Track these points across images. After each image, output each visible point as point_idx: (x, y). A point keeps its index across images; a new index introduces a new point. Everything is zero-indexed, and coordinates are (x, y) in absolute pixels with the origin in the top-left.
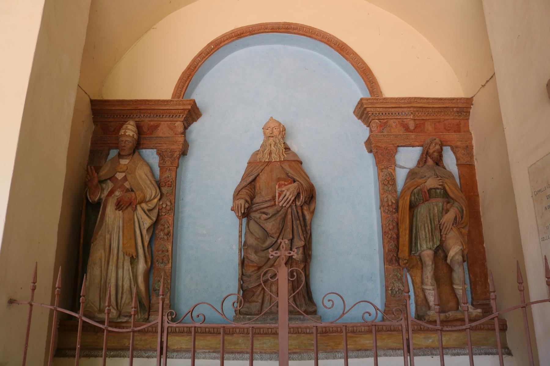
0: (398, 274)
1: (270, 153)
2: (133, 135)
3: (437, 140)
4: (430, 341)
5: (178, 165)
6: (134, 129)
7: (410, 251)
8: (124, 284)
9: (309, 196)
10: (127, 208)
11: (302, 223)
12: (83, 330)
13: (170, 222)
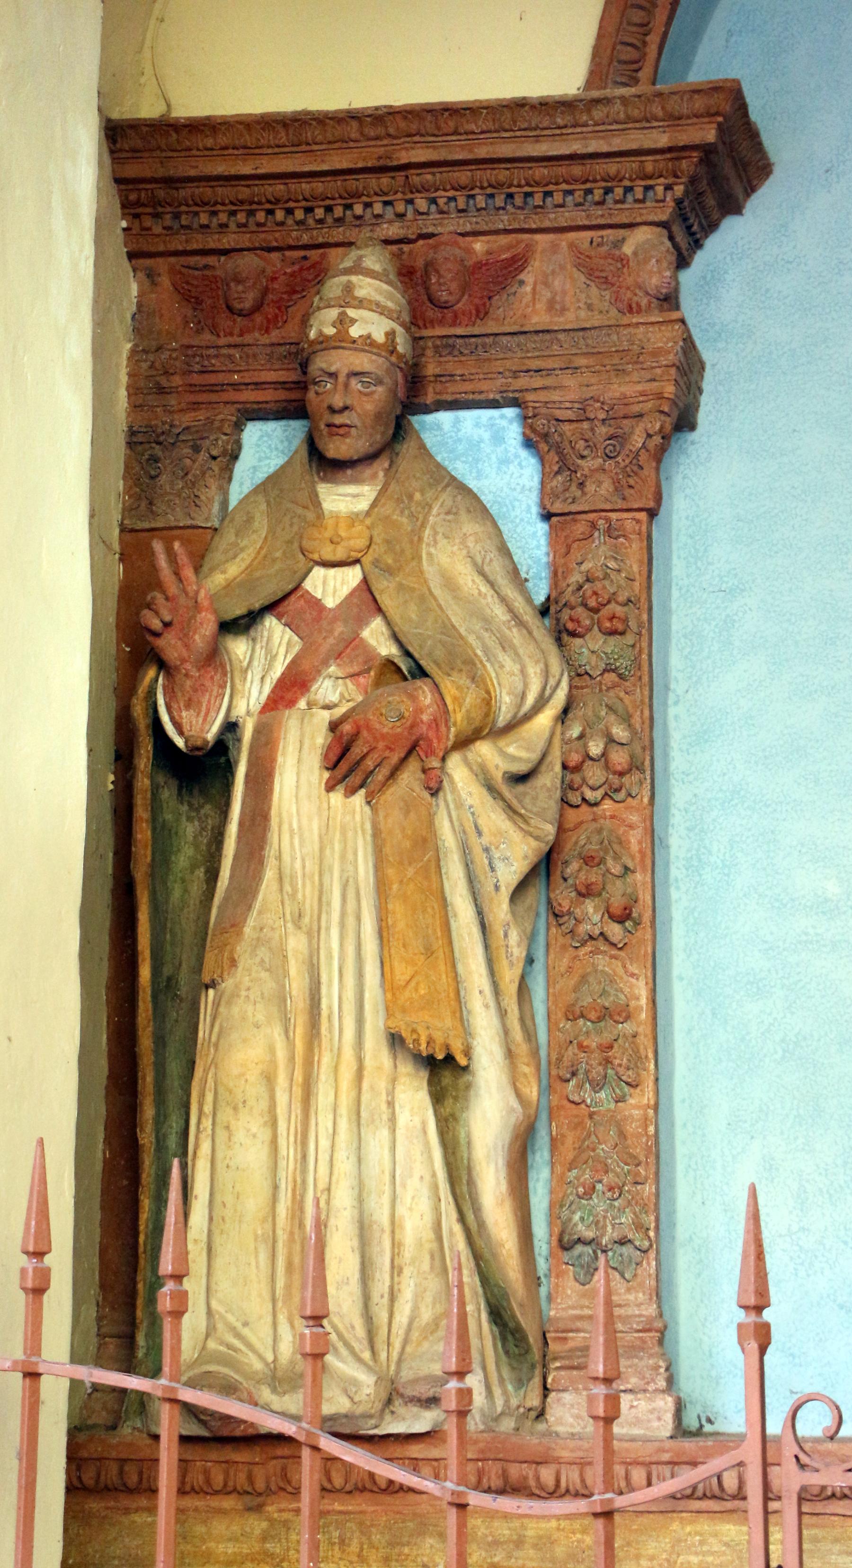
2: (391, 335)
5: (658, 498)
8: (401, 1210)
13: (634, 839)
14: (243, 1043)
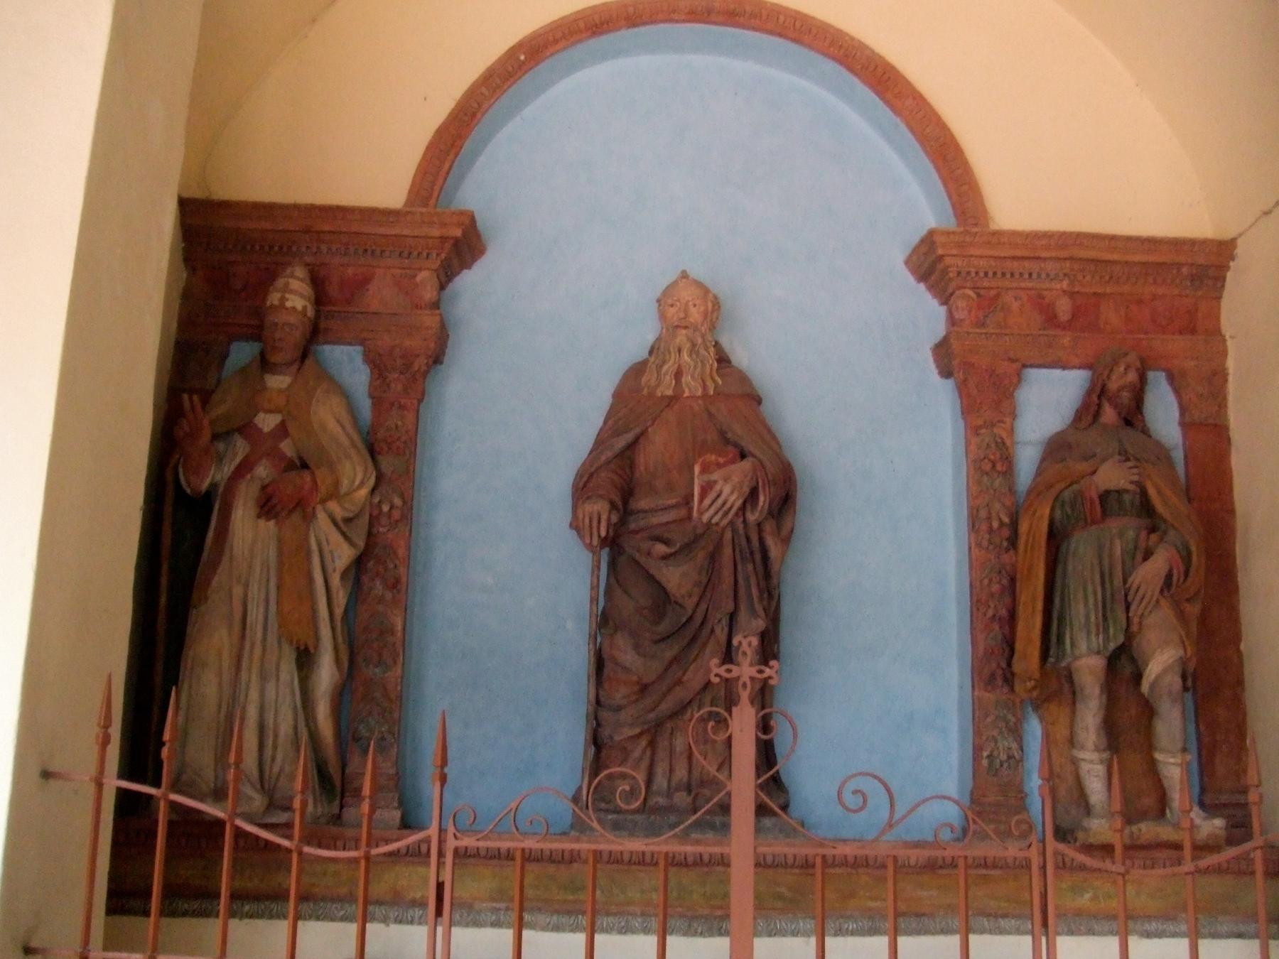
0: (1010, 717)
1: (678, 375)
2: (305, 308)
3: (1132, 358)
4: (1087, 896)
6: (307, 290)
7: (1045, 655)
9: (780, 491)
10: (291, 512)
11: (760, 568)
12: (236, 848)
13: (401, 552)
14: (211, 642)
